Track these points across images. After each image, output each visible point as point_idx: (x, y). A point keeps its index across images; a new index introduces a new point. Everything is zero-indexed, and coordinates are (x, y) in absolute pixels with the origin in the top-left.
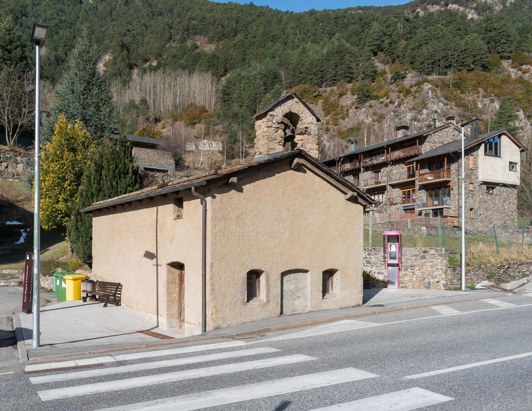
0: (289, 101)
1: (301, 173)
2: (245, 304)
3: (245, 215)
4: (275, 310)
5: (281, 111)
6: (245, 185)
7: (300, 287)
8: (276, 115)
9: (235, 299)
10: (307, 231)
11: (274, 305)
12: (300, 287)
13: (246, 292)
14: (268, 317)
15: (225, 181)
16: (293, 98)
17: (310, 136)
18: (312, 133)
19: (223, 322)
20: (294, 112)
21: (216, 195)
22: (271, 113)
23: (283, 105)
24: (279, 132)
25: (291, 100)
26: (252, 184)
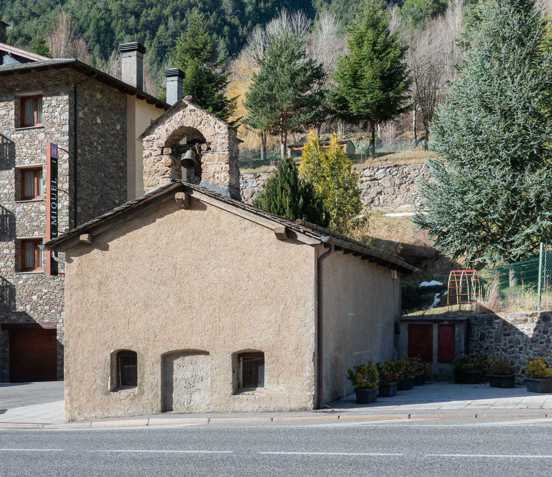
0: (177, 114)
1: (197, 212)
2: (107, 393)
3: (111, 279)
4: (152, 404)
5: (165, 131)
6: (112, 240)
7: (200, 375)
8: (156, 138)
9: (94, 386)
10: (205, 295)
11: (150, 397)
12: (200, 375)
13: (110, 378)
14: (141, 413)
15: (75, 243)
16: (186, 106)
17: (216, 154)
18: (219, 149)
19: (79, 414)
20: (188, 126)
21: (72, 258)
22: (147, 138)
23: (168, 120)
24: (163, 161)
25: (182, 111)
26: (121, 238)
